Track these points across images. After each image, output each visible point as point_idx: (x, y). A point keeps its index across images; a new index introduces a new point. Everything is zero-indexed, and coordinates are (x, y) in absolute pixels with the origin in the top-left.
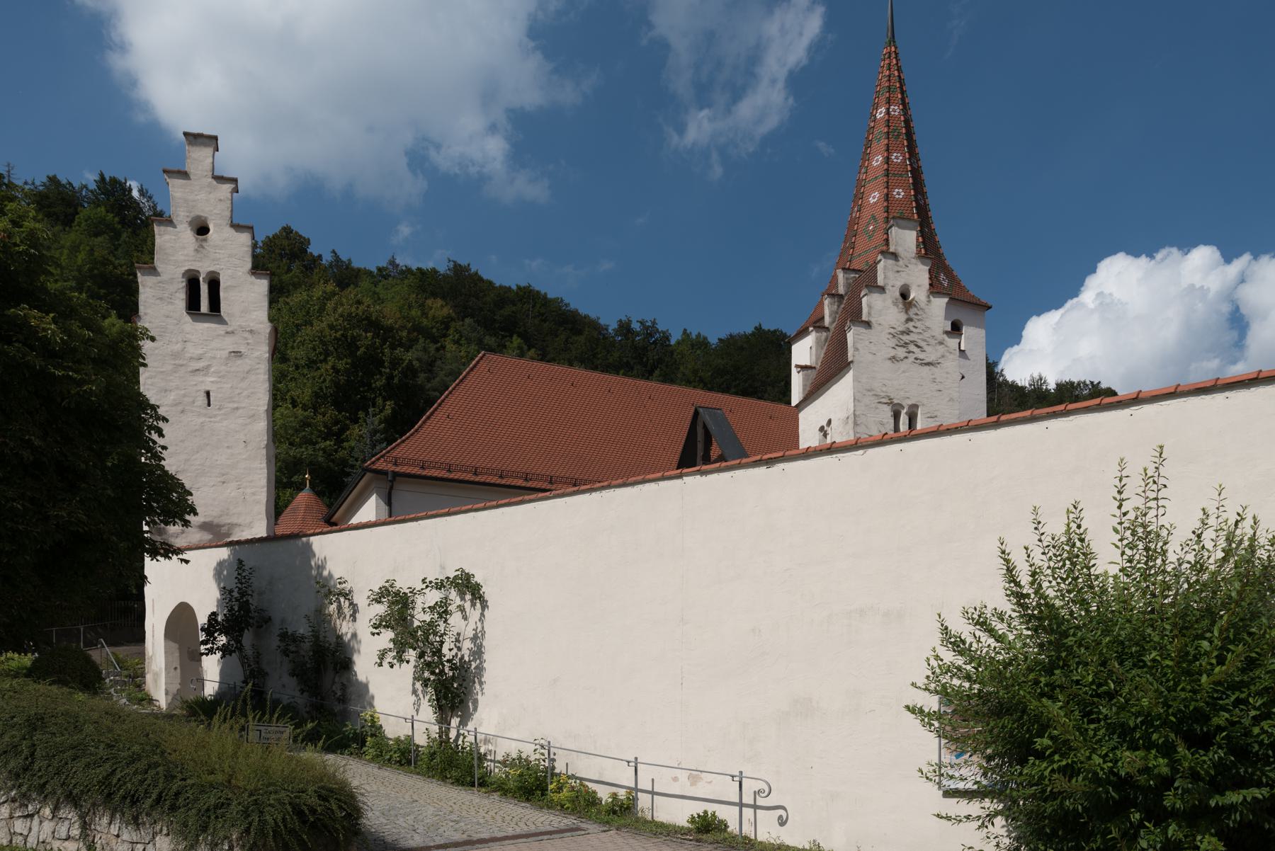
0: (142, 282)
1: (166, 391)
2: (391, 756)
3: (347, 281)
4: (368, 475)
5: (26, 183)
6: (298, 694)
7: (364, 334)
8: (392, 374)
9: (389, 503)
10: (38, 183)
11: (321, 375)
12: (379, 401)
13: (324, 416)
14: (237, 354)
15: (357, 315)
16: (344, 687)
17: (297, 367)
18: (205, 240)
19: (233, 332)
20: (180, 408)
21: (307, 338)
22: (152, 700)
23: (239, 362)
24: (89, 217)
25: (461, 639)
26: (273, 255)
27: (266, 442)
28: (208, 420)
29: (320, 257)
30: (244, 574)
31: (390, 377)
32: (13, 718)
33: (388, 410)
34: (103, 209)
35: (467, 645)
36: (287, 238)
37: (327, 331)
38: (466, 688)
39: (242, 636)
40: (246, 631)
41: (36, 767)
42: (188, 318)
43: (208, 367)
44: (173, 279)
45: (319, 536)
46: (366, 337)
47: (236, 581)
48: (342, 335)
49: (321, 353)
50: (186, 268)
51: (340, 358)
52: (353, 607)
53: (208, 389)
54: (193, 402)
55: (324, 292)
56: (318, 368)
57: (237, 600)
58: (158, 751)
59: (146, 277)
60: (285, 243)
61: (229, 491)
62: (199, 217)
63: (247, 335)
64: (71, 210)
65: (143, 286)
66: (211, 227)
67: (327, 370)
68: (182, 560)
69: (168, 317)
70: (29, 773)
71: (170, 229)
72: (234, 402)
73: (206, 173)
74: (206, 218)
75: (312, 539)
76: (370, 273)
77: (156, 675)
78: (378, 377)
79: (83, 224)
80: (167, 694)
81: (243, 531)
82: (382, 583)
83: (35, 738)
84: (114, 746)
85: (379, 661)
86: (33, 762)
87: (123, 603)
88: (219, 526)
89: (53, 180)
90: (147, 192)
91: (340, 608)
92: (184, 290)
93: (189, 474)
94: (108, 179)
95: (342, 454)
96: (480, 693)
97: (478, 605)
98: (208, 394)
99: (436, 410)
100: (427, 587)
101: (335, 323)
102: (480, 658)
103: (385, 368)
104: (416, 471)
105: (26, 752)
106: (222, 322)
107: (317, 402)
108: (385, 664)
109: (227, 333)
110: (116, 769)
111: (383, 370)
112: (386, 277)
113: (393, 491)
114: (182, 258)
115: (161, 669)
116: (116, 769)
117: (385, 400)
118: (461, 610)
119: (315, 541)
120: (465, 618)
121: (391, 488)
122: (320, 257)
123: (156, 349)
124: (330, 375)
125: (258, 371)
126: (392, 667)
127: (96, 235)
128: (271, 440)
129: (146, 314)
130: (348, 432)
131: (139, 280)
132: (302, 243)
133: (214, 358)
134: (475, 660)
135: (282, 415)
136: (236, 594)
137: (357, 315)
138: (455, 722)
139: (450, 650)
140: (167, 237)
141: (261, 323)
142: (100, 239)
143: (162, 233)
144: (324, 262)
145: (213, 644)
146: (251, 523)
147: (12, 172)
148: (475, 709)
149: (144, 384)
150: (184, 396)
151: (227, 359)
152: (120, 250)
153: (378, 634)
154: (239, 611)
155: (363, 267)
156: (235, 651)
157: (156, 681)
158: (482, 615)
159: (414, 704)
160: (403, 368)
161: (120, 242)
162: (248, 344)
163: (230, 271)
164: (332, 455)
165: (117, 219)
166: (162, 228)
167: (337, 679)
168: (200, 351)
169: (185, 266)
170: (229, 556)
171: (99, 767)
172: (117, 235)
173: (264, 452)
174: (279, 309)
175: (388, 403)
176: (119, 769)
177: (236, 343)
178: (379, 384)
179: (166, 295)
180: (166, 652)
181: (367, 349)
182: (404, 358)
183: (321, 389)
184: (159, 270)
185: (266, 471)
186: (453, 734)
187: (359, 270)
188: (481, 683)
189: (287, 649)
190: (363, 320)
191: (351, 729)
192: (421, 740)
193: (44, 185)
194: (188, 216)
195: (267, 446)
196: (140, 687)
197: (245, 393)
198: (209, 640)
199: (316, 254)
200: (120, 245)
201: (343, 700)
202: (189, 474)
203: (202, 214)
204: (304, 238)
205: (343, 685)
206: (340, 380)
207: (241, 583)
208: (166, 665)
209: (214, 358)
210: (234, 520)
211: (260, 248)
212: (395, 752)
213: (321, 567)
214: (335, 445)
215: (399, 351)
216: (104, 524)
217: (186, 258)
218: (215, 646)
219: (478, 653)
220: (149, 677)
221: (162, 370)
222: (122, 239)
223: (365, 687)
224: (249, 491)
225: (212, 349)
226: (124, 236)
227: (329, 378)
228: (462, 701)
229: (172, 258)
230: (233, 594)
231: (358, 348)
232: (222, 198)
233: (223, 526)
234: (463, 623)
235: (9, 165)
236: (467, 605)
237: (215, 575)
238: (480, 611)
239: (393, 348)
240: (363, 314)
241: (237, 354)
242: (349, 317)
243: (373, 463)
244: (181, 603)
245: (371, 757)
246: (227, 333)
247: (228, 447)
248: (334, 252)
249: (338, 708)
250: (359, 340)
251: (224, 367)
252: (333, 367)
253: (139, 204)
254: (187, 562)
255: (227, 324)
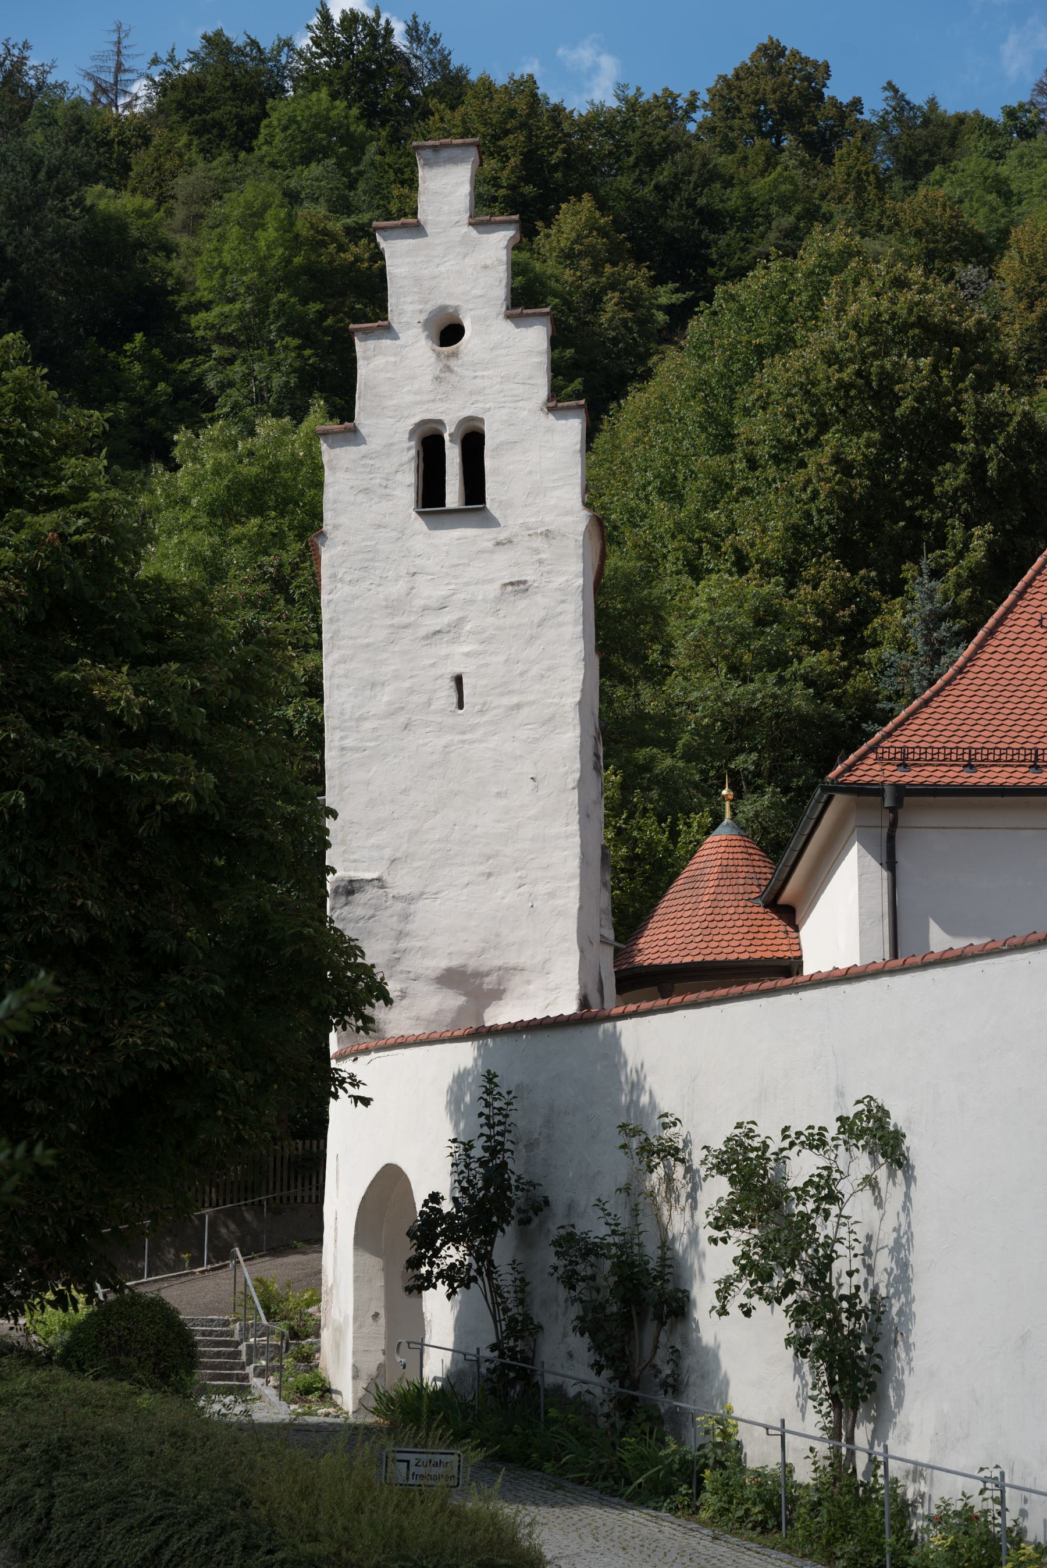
0: (330, 461)
1: (373, 685)
2: (747, 1510)
3: (926, 157)
4: (839, 801)
5: (155, 61)
6: (590, 1375)
7: (910, 362)
8: (983, 455)
9: (890, 864)
10: (181, 55)
11: (809, 481)
12: (956, 532)
13: (815, 588)
14: (518, 586)
15: (894, 316)
16: (676, 1356)
17: (753, 464)
18: (455, 355)
19: (510, 542)
20: (402, 719)
21: (774, 387)
22: (329, 1390)
23: (522, 603)
24: (292, 120)
25: (873, 1248)
26: (736, 122)
27: (577, 775)
28: (458, 738)
29: (856, 104)
30: (496, 1104)
31: (979, 465)
32: (24, 1447)
33: (978, 553)
34: (324, 93)
35: (883, 1261)
36: (773, 70)
37: (821, 370)
38: (879, 1356)
39: (491, 1243)
40: (499, 1233)
41: (52, 1535)
42: (419, 524)
43: (460, 622)
44: (391, 445)
45: (634, 1020)
46: (918, 370)
47: (483, 1120)
48: (859, 373)
49: (806, 426)
50: (417, 419)
51: (854, 430)
52: (693, 1178)
53: (458, 670)
54: (429, 703)
55: (825, 254)
56: (802, 464)
57: (483, 1163)
58: (239, 1502)
59: (337, 450)
60: (767, 84)
61: (500, 893)
62: (443, 309)
63: (538, 543)
64: (253, 109)
65: (333, 469)
66: (467, 324)
67: (820, 468)
68: (357, 1099)
69: (379, 526)
70: (43, 1546)
71: (386, 343)
72: (510, 692)
73: (457, 218)
74: (457, 309)
75: (620, 1024)
76: (987, 127)
77: (339, 1330)
78: (948, 466)
79: (280, 136)
80: (355, 1377)
81: (529, 982)
82: (730, 1131)
83: (55, 1483)
84: (171, 1495)
85: (718, 1305)
86: (48, 1528)
87: (300, 1143)
88: (478, 975)
89: (216, 43)
90: (428, 30)
91: (669, 1179)
92: (413, 466)
93: (417, 864)
94: (337, 17)
95: (860, 681)
96: (906, 1373)
97: (900, 1173)
98: (458, 680)
99: (1010, 610)
100: (792, 1144)
101: (838, 346)
102: (907, 1291)
103: (964, 441)
104: (955, 776)
105: (39, 1508)
106: (490, 522)
107: (797, 552)
108: (733, 1307)
109: (498, 544)
110: (171, 1536)
111: (959, 447)
112: (1027, 133)
113: (899, 832)
114: (409, 398)
115: (346, 1317)
116: (171, 1536)
117: (969, 523)
118: (871, 1185)
119: (624, 1027)
120: (879, 1203)
121: (893, 825)
122: (856, 104)
123: (355, 597)
124: (828, 480)
125: (561, 618)
126: (747, 1314)
127: (306, 160)
128: (590, 766)
129: (336, 527)
130: (877, 622)
131: (325, 459)
132: (809, 78)
133: (472, 602)
134: (897, 1295)
135: (711, 600)
136: (477, 1152)
137: (894, 316)
138: (862, 1434)
139: (850, 1274)
140: (379, 361)
141: (567, 513)
142: (315, 169)
143: (370, 353)
144: (866, 116)
145: (432, 1264)
146: (546, 962)
147: (125, 42)
148: (900, 1403)
149: (331, 677)
150: (411, 691)
151: (499, 599)
152: (361, 186)
153: (724, 1240)
154: (486, 1187)
155: (970, 110)
156: (474, 1279)
157: (337, 1345)
158: (907, 1196)
159: (798, 1396)
160: (1009, 436)
161: (361, 168)
162: (541, 562)
163: (504, 411)
164: (837, 686)
165: (355, 111)
166: (371, 344)
167: (663, 1338)
168: (443, 591)
169: (414, 415)
170: (475, 1060)
171: (146, 1532)
172: (356, 147)
173: (574, 797)
174: (715, 313)
175: (977, 531)
176: (176, 1536)
177: (516, 564)
178: (949, 484)
179: (378, 481)
180: (356, 1279)
181: (919, 399)
182: (1010, 410)
183: (808, 515)
184: (363, 431)
185: (577, 840)
186: (861, 1462)
187: (961, 119)
188: (908, 1348)
189: (574, 1272)
190: (912, 326)
191: (675, 1452)
192: (804, 1474)
193: (194, 57)
194: (421, 311)
195: (581, 783)
196: (308, 1359)
197: (535, 671)
198: (424, 1256)
199: (845, 99)
200: (361, 173)
201: (675, 1386)
202: (417, 864)
203: (448, 302)
204: (815, 64)
205: (675, 1351)
206: (852, 490)
207: (491, 1126)
208: (356, 1309)
209: (472, 602)
210: (511, 959)
211: (706, 106)
212: (754, 1504)
213: (637, 1087)
214: (843, 658)
215: (997, 396)
216: (209, 1047)
217: (418, 398)
218: (436, 1270)
219: (903, 1277)
220: (326, 1335)
221: (367, 641)
222: (366, 158)
223: (712, 1356)
224: (542, 889)
225: (467, 584)
226: (372, 148)
227: (824, 488)
228: (872, 1387)
229: (391, 403)
230: (472, 1153)
231: (898, 400)
232: (489, 262)
233: (488, 974)
234: (875, 1213)
235: (119, 29)
236: (882, 1174)
237: (449, 1103)
238: (904, 1189)
239: (982, 386)
240: (910, 311)
241: (518, 586)
242: (872, 328)
243: (849, 769)
244: (387, 1165)
245: (709, 1514)
246: (498, 544)
247: (499, 795)
248: (890, 86)
249: (664, 1402)
250: (900, 381)
251: (490, 620)
252: (836, 459)
253: (408, 62)
254: (366, 1101)
255: (498, 525)
